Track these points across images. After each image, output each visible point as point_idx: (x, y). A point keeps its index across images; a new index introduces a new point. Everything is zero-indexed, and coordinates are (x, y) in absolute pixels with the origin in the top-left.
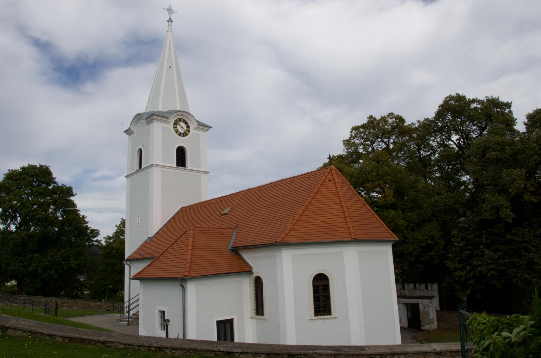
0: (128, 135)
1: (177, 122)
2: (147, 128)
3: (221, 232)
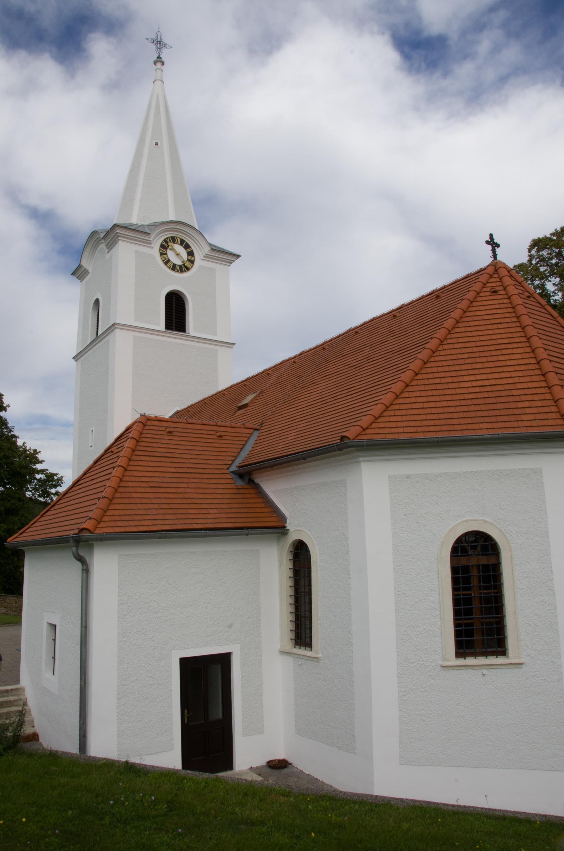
1: (167, 243)
2: (108, 256)
3: (218, 434)
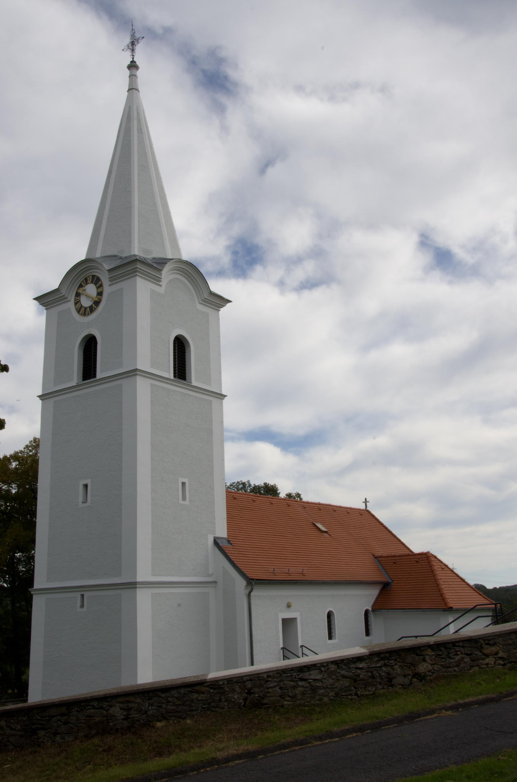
0: (45, 308)
